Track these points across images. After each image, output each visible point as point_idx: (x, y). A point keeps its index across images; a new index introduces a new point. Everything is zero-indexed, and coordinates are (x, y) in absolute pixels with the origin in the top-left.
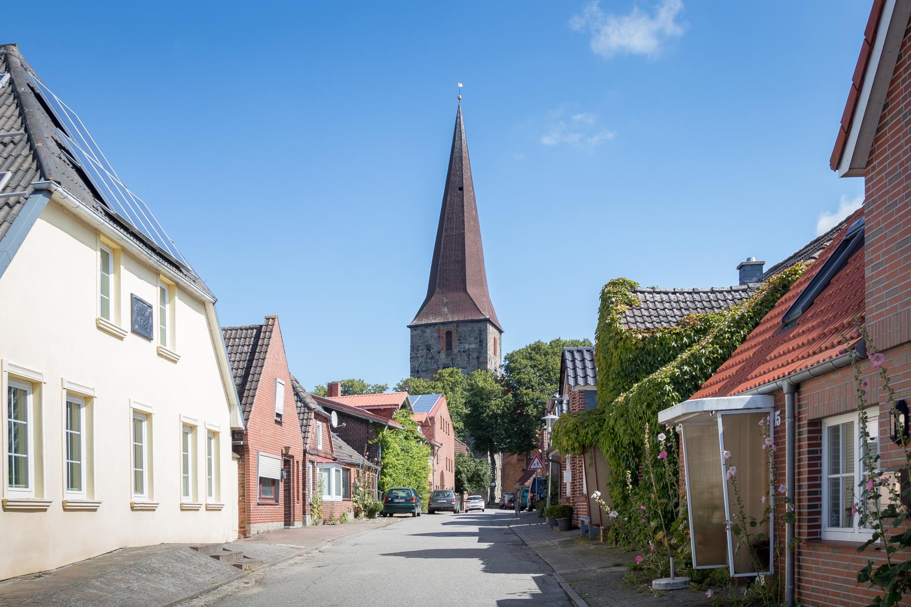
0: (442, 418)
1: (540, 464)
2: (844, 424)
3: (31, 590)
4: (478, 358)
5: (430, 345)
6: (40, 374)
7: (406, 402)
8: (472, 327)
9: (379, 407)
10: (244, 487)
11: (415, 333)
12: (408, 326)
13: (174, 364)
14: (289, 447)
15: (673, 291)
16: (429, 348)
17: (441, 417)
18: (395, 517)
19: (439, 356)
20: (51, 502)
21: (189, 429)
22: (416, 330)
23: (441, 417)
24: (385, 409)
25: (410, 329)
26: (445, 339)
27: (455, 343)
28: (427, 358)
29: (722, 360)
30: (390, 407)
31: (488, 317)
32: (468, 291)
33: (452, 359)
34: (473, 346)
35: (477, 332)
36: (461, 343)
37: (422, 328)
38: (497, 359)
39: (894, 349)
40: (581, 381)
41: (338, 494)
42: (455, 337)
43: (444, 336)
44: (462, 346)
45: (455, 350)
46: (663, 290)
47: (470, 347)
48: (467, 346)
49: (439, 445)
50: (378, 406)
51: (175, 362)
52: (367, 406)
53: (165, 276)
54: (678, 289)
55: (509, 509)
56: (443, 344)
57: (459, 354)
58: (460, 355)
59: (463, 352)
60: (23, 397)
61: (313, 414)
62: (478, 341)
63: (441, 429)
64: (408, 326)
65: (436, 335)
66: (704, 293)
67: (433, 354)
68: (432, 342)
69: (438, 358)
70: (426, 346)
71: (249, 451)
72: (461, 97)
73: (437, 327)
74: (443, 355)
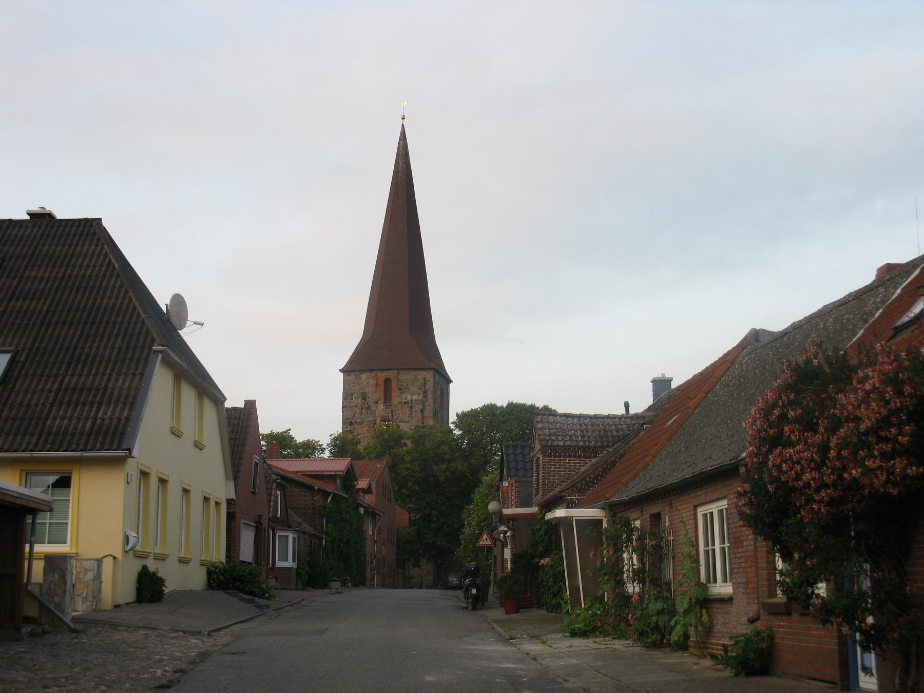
0: (384, 483)
1: (488, 541)
2: (151, 601)
3: (286, 589)
5: (366, 393)
6: (150, 468)
7: (350, 468)
8: (416, 376)
9: (323, 473)
11: (349, 378)
12: (340, 370)
13: (200, 451)
14: (262, 516)
16: (364, 397)
17: (383, 482)
19: (377, 407)
20: (168, 555)
21: (206, 499)
22: (349, 375)
23: (383, 482)
25: (342, 374)
26: (383, 388)
27: (395, 392)
28: (362, 409)
29: (818, 357)
33: (392, 411)
35: (422, 381)
36: (403, 393)
37: (356, 373)
41: (294, 560)
42: (394, 384)
43: (382, 383)
44: (404, 396)
45: (395, 401)
49: (382, 514)
50: (322, 471)
51: (201, 450)
55: (670, 421)
56: (381, 393)
57: (400, 405)
58: (401, 407)
60: (545, 564)
61: (275, 484)
63: (383, 495)
64: (340, 370)
65: (373, 382)
68: (370, 390)
69: (375, 409)
71: (236, 519)
73: (374, 373)
74: (381, 406)
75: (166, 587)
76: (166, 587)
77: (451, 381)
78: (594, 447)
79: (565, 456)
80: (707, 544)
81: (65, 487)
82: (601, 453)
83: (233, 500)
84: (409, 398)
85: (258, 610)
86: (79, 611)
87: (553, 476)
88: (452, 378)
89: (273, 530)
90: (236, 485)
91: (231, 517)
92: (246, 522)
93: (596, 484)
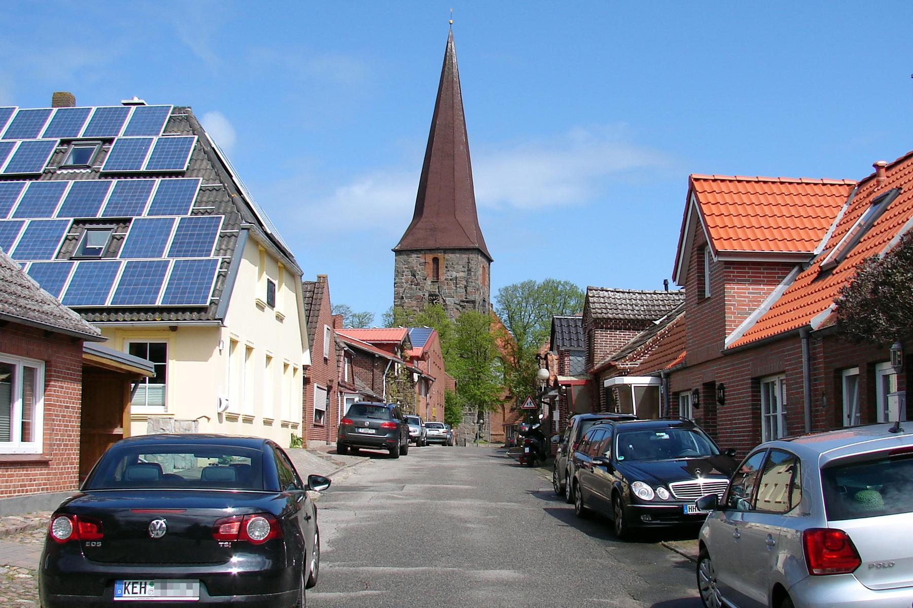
1: (532, 404)
4: (466, 287)
7: (407, 339)
9: (383, 342)
10: (305, 411)
12: (392, 250)
15: (628, 291)
18: (78, 525)
21: (286, 366)
24: (387, 344)
30: (392, 342)
31: (477, 246)
32: (457, 218)
34: (462, 274)
36: (449, 271)
38: (486, 289)
39: (679, 373)
40: (567, 343)
43: (431, 262)
44: (449, 274)
46: (621, 290)
47: (458, 276)
48: (454, 274)
49: (433, 380)
52: (370, 340)
53: (262, 246)
54: (633, 290)
59: (451, 280)
61: (343, 352)
62: (466, 269)
64: (392, 250)
66: (649, 294)
67: (419, 281)
70: (411, 271)
72: (451, 22)
75: (545, 509)
76: (545, 509)
77: (492, 261)
78: (642, 320)
79: (616, 329)
80: (768, 411)
81: (908, 413)
82: (649, 326)
83: (308, 366)
84: (454, 276)
85: (335, 466)
86: (179, 468)
87: (605, 346)
88: (493, 258)
89: (341, 393)
90: (311, 352)
91: (306, 381)
92: (320, 386)
93: (646, 353)
